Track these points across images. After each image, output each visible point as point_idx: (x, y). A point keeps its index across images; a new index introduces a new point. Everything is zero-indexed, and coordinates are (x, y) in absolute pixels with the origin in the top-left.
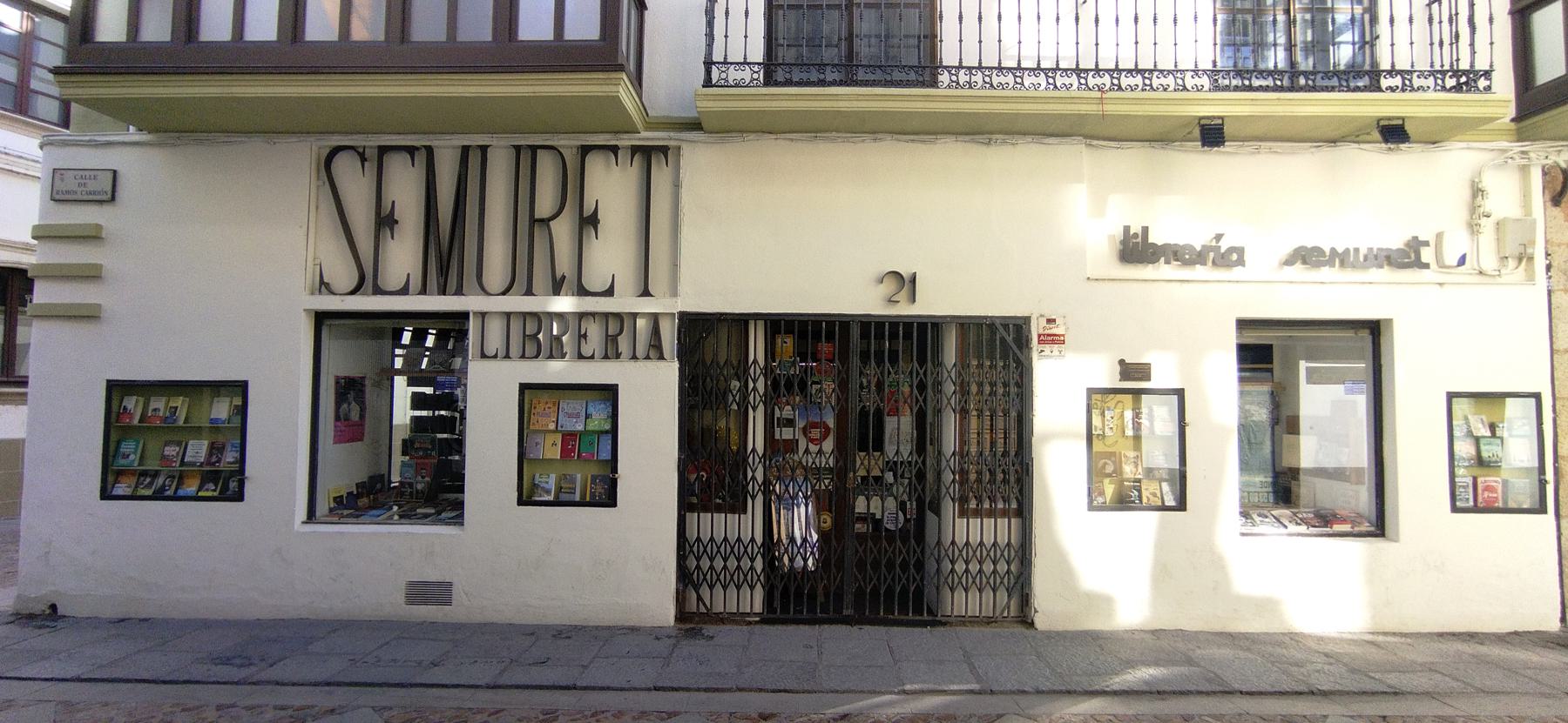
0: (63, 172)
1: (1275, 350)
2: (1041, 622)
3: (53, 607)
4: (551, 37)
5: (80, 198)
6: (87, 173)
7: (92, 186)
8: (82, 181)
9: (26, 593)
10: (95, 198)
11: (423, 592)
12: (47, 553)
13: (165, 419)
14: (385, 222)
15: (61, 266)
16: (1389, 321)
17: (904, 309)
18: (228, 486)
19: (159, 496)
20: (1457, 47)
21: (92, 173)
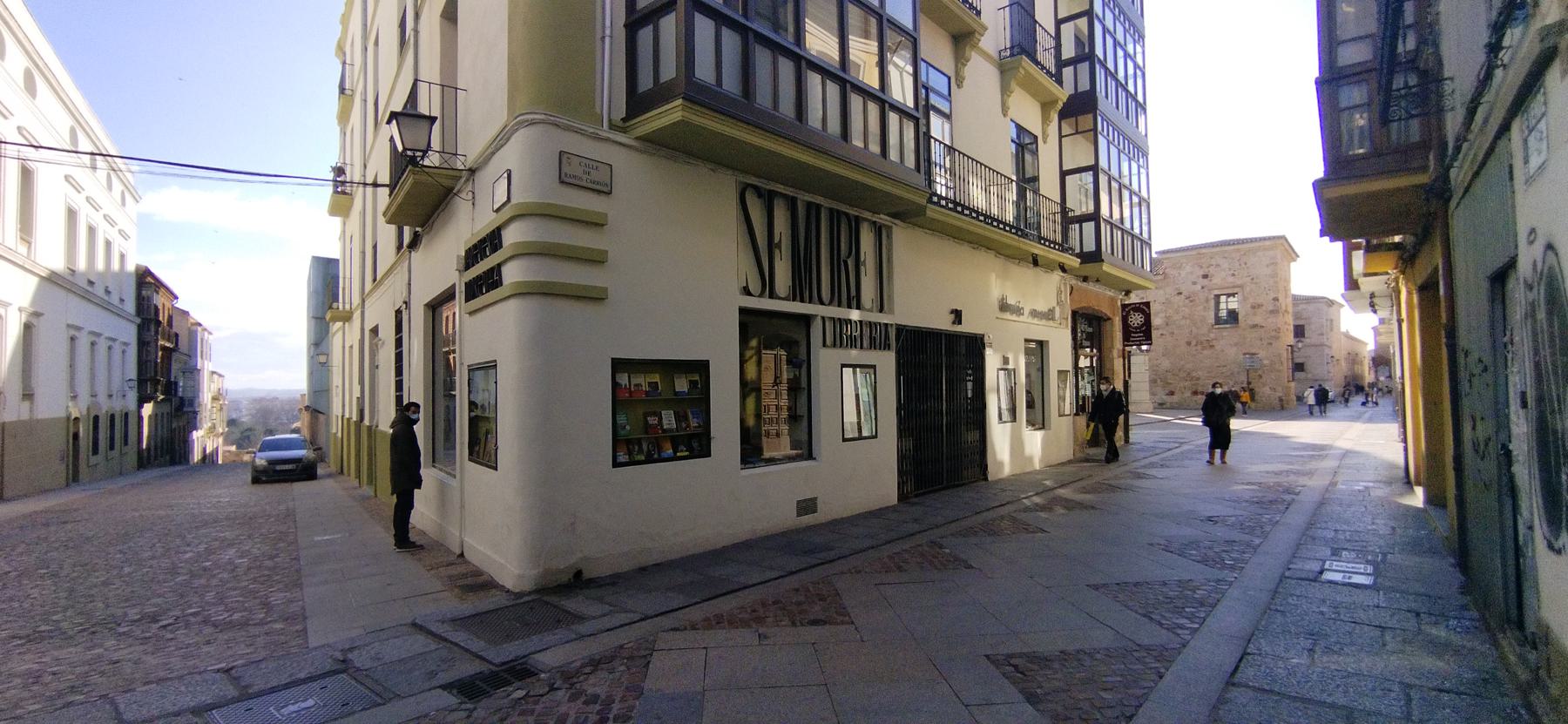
0: (570, 156)
1: (1297, 324)
2: (989, 479)
3: (578, 574)
4: (1079, 118)
5: (584, 184)
6: (591, 163)
7: (595, 175)
8: (587, 169)
9: (1466, 467)
10: (598, 187)
11: (807, 507)
12: (572, 524)
13: (647, 393)
14: (772, 246)
15: (569, 247)
16: (1047, 342)
17: (958, 328)
18: (693, 447)
19: (649, 460)
20: (363, 313)
21: (595, 164)
